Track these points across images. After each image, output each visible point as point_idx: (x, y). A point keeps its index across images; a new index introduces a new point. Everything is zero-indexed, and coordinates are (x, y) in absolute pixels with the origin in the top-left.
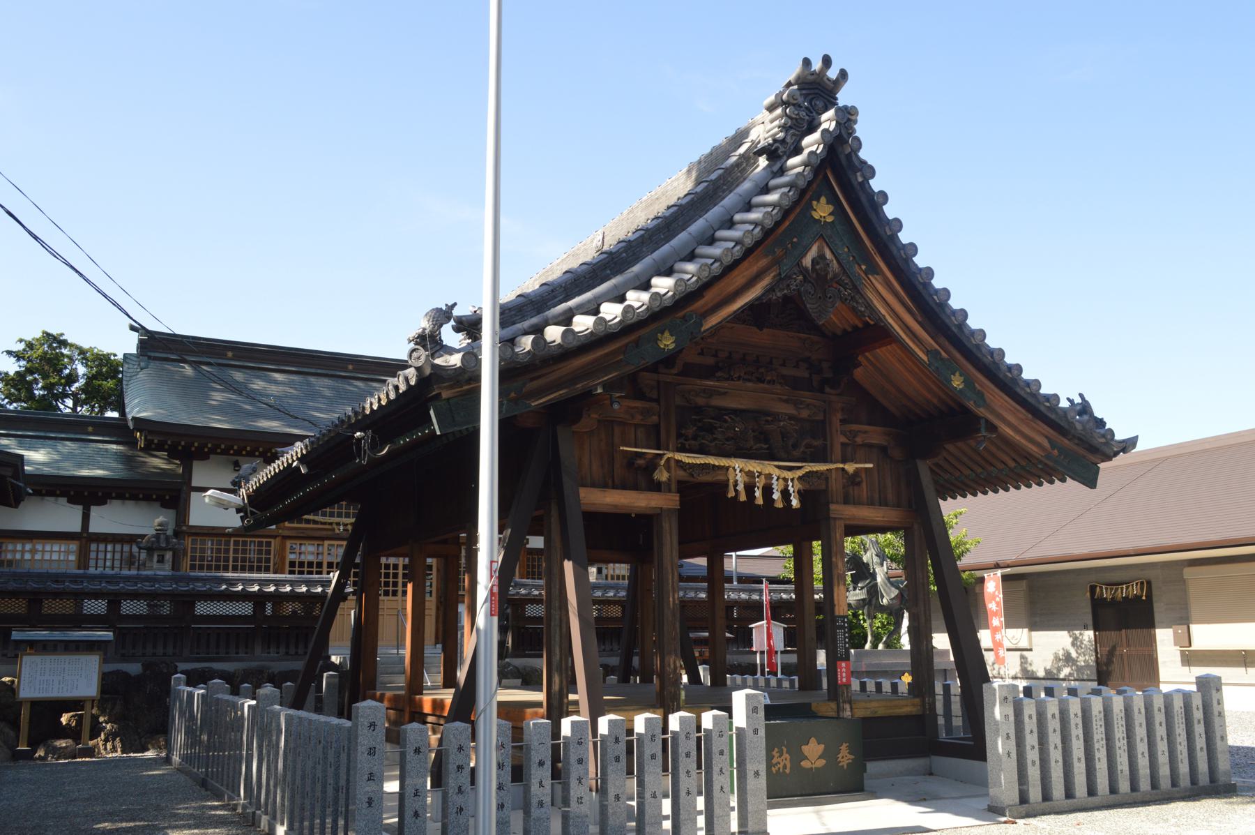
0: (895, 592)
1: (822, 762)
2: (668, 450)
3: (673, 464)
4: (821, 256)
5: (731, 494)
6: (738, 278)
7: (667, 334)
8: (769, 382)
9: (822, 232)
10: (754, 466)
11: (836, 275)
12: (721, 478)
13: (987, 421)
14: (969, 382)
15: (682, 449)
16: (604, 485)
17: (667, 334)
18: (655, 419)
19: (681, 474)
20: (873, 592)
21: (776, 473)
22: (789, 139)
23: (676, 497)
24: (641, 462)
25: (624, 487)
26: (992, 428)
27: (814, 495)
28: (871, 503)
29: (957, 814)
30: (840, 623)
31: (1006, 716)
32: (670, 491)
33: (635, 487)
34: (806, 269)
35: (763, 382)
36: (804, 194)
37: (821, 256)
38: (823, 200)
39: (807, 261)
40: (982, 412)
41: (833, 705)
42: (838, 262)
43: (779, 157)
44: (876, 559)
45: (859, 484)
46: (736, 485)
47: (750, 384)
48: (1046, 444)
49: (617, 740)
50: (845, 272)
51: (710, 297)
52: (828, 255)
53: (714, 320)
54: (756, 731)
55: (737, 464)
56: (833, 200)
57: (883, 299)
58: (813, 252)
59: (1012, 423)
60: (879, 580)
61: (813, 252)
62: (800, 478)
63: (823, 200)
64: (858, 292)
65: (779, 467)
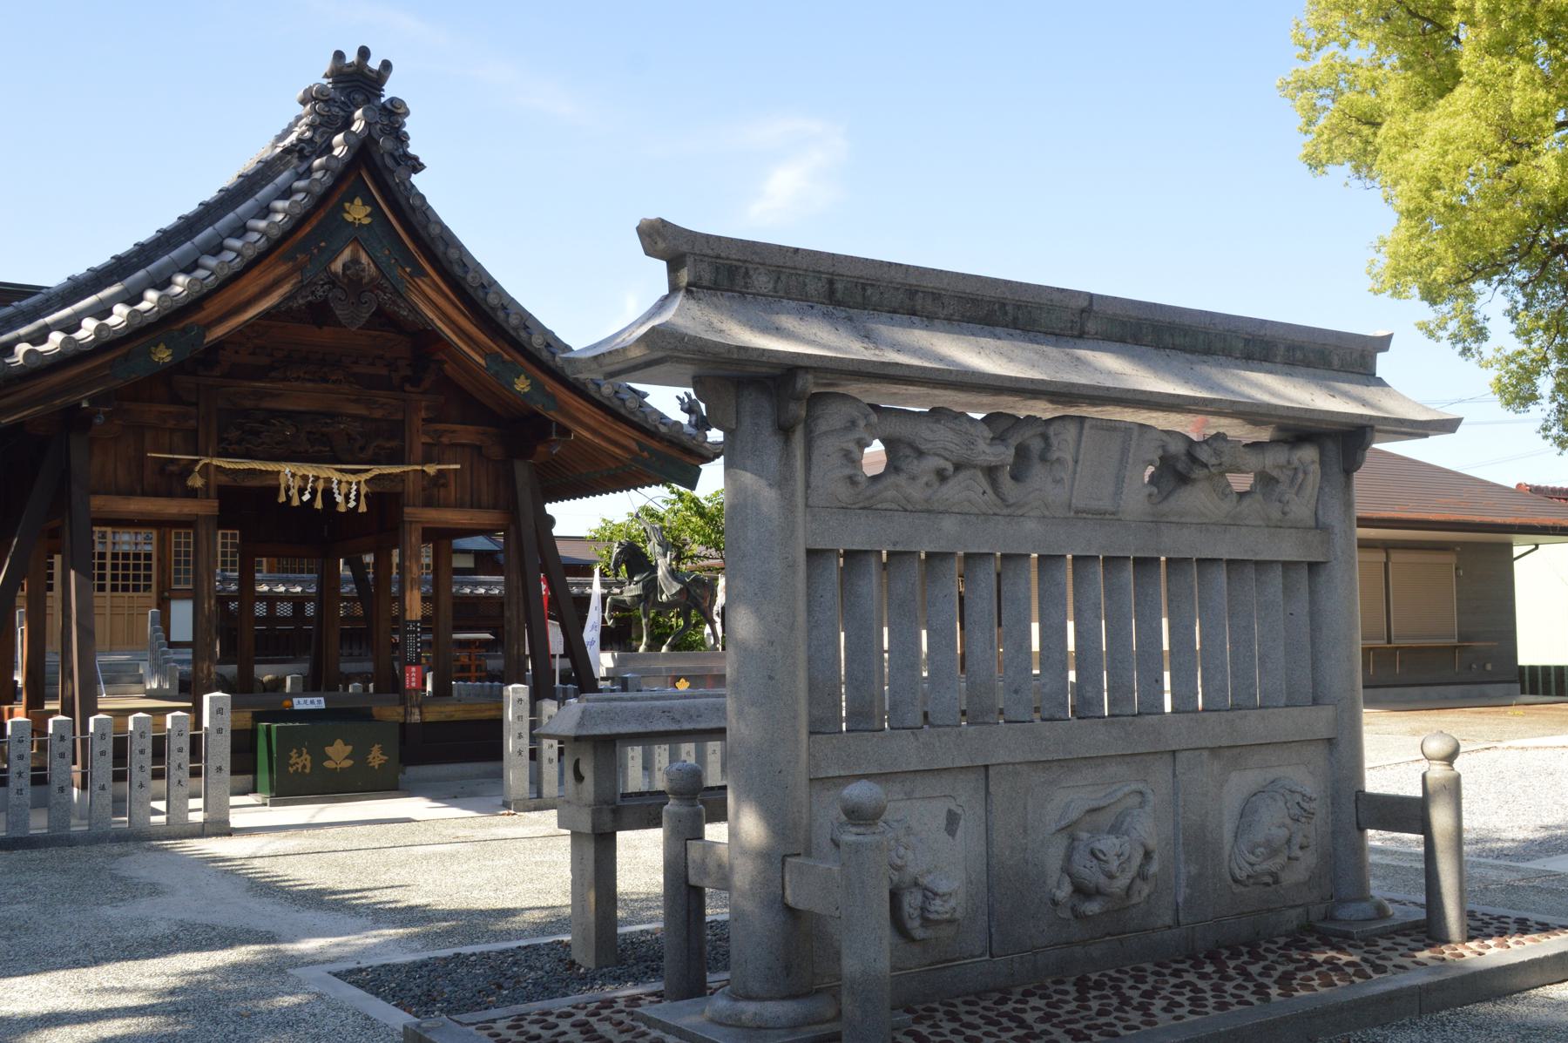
0: (676, 587)
1: (349, 763)
2: (207, 455)
3: (212, 469)
4: (355, 261)
5: (282, 499)
6: (249, 286)
7: (162, 347)
8: (334, 382)
9: (357, 235)
10: (310, 470)
11: (372, 279)
12: (273, 483)
13: (558, 424)
14: (535, 384)
15: (220, 455)
16: (130, 493)
17: (162, 347)
18: (193, 422)
19: (223, 479)
20: (651, 587)
21: (335, 477)
22: (317, 139)
23: (216, 503)
24: (173, 468)
25: (156, 494)
26: (565, 432)
27: (385, 500)
28: (459, 505)
29: (434, 799)
30: (411, 627)
31: (520, 718)
32: (208, 497)
33: (170, 494)
34: (335, 275)
35: (327, 382)
36: (326, 203)
37: (355, 261)
38: (358, 201)
39: (337, 266)
40: (553, 415)
41: (401, 710)
42: (376, 266)
43: (307, 158)
44: (658, 549)
45: (445, 485)
46: (288, 489)
47: (309, 385)
48: (634, 446)
49: (62, 738)
50: (384, 276)
51: (212, 308)
52: (364, 259)
53: (219, 331)
54: (220, 731)
55: (287, 469)
56: (369, 200)
57: (431, 304)
58: (346, 255)
59: (587, 428)
60: (660, 573)
61: (346, 255)
62: (366, 481)
63: (358, 201)
64: (401, 296)
65: (341, 471)
